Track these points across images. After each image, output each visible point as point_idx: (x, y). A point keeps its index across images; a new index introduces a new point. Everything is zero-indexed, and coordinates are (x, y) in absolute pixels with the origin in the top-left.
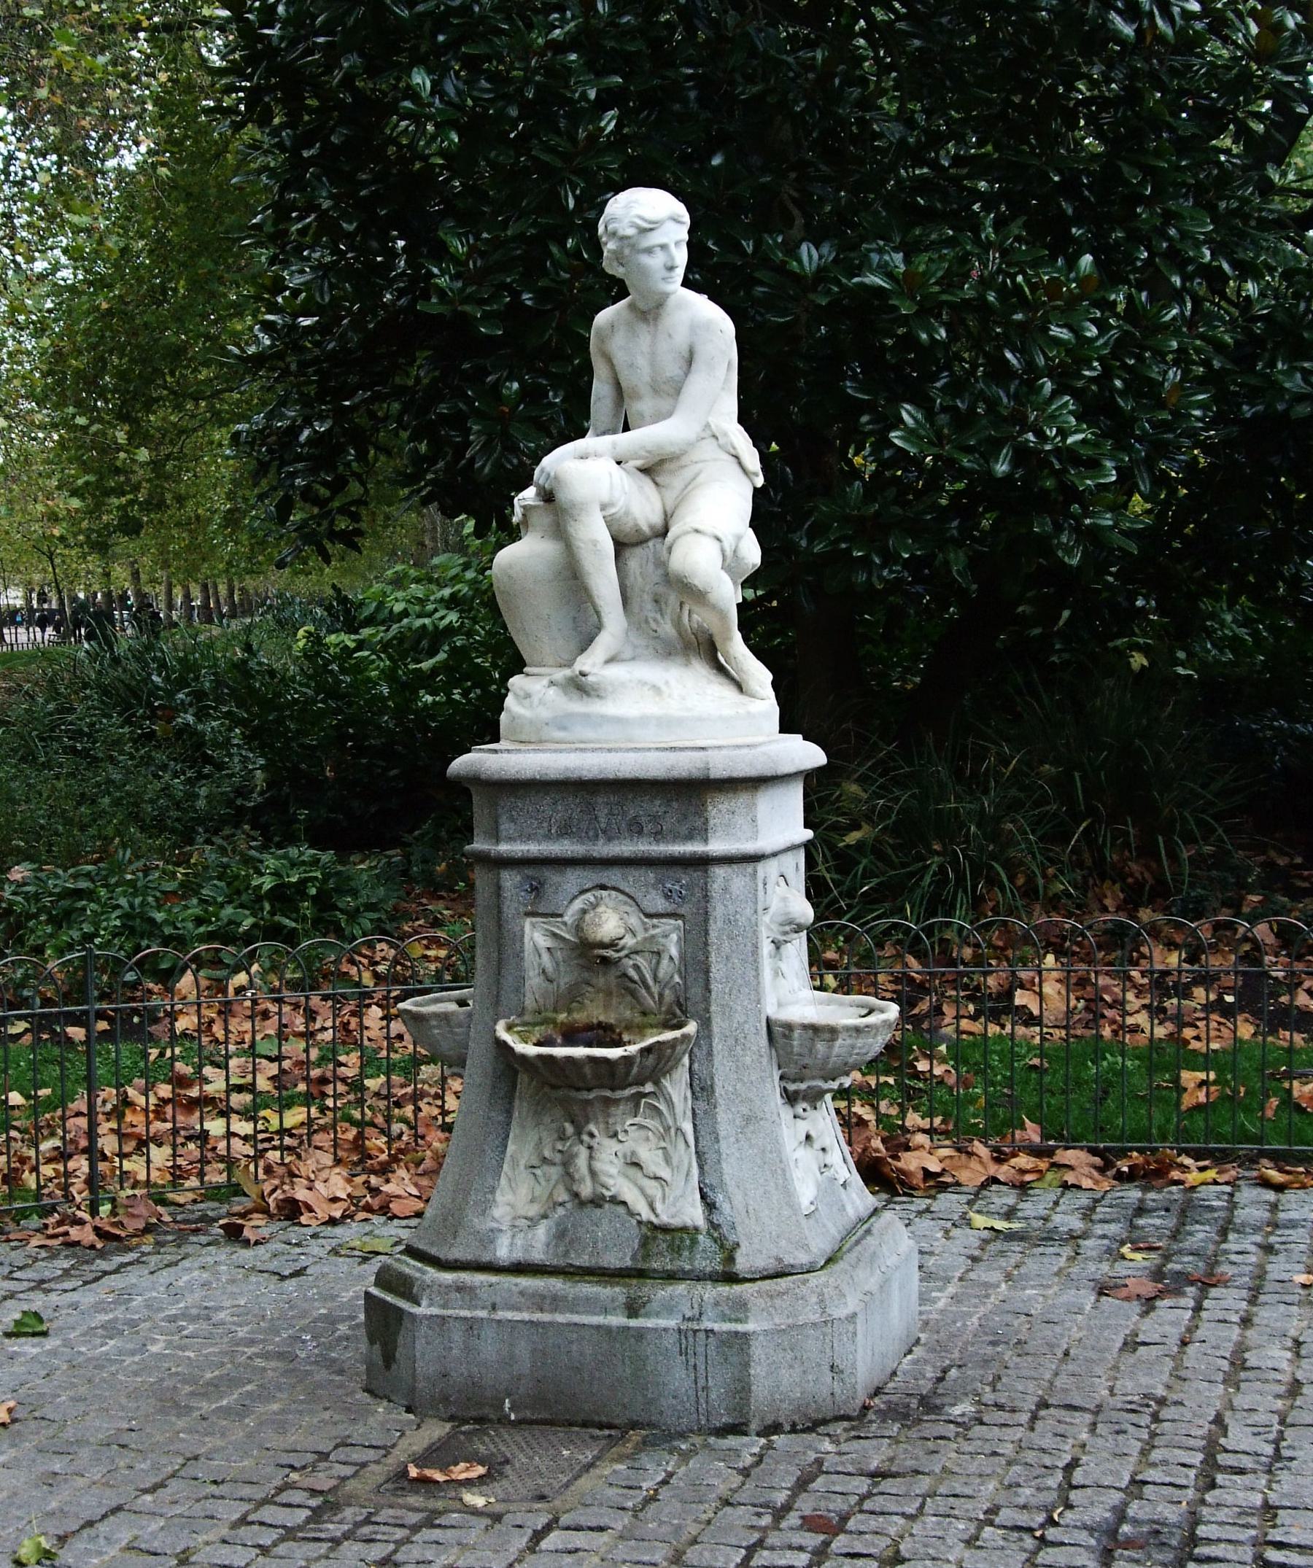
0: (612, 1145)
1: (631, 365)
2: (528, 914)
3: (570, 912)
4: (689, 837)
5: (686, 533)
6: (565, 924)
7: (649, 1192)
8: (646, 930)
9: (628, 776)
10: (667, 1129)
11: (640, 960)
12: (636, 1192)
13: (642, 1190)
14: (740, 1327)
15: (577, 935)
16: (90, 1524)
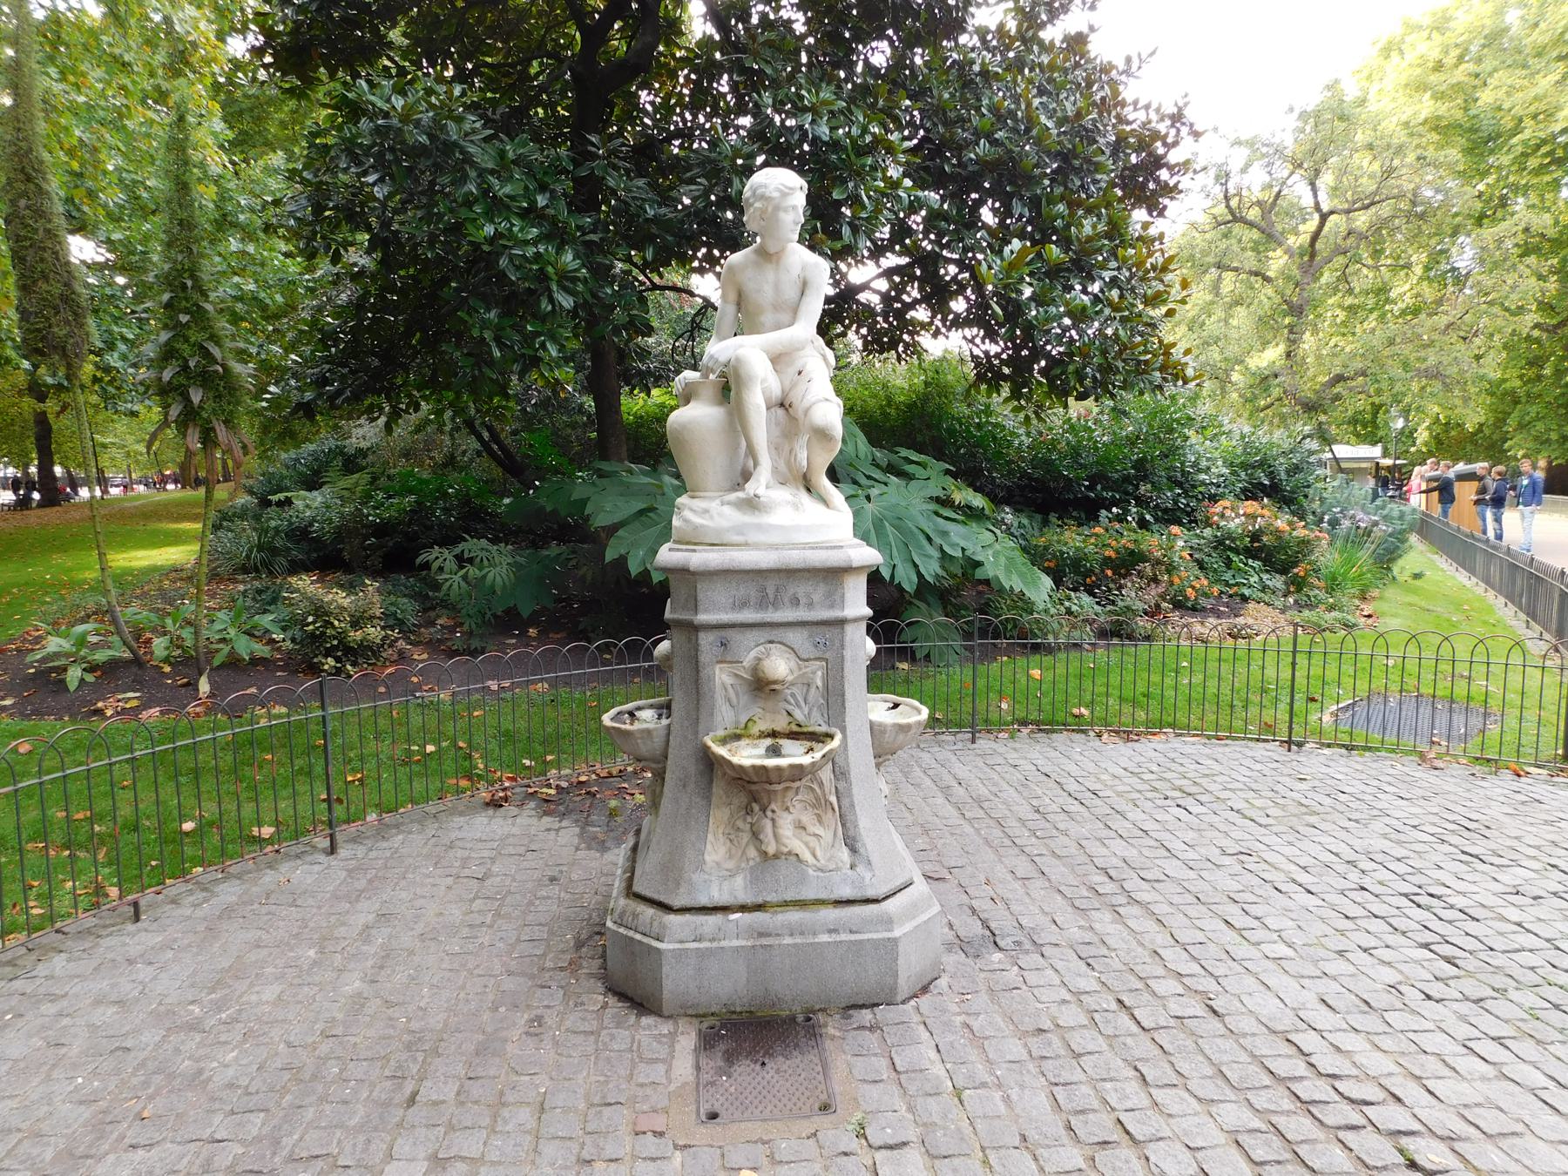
0: (785, 814)
4: (832, 606)
9: (836, 564)
11: (795, 690)
13: (806, 844)
14: (889, 935)
16: (1279, 1162)
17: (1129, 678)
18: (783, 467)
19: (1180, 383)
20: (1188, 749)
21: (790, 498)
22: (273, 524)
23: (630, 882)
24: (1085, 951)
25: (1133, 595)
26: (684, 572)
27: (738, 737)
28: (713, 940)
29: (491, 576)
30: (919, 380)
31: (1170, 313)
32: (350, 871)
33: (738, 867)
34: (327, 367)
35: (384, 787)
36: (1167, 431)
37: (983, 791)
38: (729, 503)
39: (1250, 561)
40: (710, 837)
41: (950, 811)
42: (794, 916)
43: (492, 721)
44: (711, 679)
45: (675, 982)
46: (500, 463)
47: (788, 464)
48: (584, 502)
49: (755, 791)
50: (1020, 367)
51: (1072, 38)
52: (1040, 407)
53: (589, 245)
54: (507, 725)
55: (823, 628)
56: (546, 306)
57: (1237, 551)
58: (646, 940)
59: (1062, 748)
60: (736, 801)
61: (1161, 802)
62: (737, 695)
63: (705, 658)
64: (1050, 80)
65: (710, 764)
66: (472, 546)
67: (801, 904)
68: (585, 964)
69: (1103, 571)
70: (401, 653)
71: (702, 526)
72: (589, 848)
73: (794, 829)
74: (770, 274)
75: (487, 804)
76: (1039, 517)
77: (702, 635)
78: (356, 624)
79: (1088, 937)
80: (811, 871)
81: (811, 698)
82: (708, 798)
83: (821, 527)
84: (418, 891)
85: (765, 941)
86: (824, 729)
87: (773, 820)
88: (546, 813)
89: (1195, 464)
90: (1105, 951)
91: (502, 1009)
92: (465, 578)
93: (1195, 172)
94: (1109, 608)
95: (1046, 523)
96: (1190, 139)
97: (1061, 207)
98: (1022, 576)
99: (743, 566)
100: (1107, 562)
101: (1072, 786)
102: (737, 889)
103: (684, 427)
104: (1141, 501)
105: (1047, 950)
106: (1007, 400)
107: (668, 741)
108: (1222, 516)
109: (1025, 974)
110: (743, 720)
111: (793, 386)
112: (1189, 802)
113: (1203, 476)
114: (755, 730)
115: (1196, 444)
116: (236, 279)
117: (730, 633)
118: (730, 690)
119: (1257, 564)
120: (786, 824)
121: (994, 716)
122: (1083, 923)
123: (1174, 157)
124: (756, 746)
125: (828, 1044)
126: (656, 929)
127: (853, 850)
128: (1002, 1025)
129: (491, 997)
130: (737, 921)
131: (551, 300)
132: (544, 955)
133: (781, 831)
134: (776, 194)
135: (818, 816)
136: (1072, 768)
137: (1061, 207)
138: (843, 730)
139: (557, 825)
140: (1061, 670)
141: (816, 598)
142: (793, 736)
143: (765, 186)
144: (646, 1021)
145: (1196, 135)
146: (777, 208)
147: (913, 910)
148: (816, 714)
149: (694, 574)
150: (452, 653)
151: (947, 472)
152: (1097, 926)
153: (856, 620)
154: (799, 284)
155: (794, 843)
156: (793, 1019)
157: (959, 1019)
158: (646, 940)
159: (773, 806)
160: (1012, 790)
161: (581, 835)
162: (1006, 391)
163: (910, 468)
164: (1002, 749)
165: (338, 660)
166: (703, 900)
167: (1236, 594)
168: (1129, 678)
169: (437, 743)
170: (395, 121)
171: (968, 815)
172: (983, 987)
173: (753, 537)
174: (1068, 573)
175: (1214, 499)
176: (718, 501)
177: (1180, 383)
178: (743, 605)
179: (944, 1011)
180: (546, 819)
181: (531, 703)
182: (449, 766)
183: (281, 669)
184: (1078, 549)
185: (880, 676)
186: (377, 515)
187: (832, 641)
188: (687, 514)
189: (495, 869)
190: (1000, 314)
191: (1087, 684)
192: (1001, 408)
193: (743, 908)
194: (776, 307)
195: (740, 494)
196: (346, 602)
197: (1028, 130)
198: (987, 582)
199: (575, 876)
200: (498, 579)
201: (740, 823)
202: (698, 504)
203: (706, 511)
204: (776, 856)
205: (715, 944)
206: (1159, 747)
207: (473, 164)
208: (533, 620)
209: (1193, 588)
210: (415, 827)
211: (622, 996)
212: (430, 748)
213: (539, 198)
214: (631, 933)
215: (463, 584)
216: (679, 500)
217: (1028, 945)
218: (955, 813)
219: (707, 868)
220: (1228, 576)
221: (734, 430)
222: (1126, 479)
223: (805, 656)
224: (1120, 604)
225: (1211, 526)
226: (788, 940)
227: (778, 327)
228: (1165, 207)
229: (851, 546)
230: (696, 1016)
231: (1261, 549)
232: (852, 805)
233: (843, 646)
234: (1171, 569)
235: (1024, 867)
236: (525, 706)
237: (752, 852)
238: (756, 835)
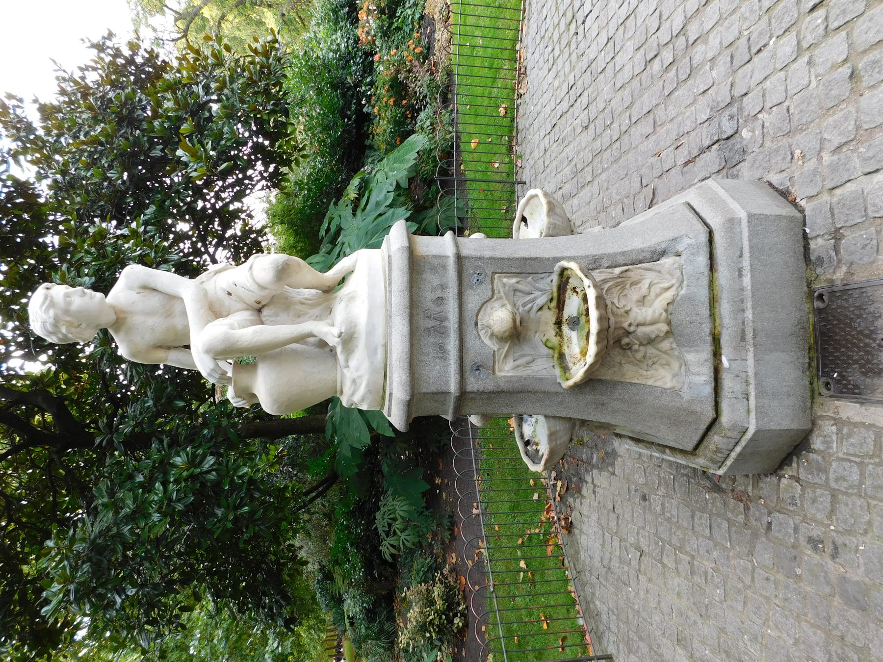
0: (632, 314)
1: (153, 330)
2: (494, 373)
3: (492, 346)
4: (444, 267)
5: (252, 275)
6: (499, 349)
7: (658, 291)
8: (501, 298)
9: (406, 262)
10: (617, 285)
11: (519, 303)
12: (660, 299)
13: (658, 296)
15: (506, 342)
17: (477, 81)
18: (316, 311)
19: (277, 45)
20: (533, 29)
21: (343, 304)
22: (363, 630)
23: (683, 452)
24: (742, 55)
25: (420, 84)
26: (409, 405)
27: (562, 356)
28: (747, 383)
29: (402, 513)
30: (278, 228)
31: (228, 49)
32: (630, 651)
33: (678, 358)
34: (261, 610)
35: (553, 603)
36: (314, 70)
37: (567, 171)
38: (347, 361)
39: (397, 15)
40: (650, 382)
41: (586, 193)
42: (725, 308)
43: (502, 519)
44: (509, 379)
45: (785, 419)
46: (331, 485)
47: (313, 306)
48: (352, 448)
49: (616, 341)
50: (268, 157)
51: (42, 115)
52: (295, 148)
53: (170, 446)
54: (506, 507)
55: (464, 275)
56: (213, 476)
57: (391, 24)
58: (743, 443)
59: (531, 120)
60: (618, 359)
61: (580, 37)
62: (523, 356)
63: (490, 386)
64: (69, 129)
65: (590, 381)
66: (380, 522)
67: (713, 301)
68: (741, 488)
69: (403, 106)
70: (451, 571)
71: (367, 386)
72: (613, 465)
73: (648, 303)
74: (137, 320)
75: (570, 532)
76: (367, 152)
77: (469, 388)
78: (431, 603)
79: (725, 58)
80: (683, 292)
81: (527, 289)
82: (615, 384)
83: (371, 275)
84: (653, 605)
85: (749, 335)
86: (555, 277)
87: (638, 325)
88: (579, 491)
89: (335, 52)
90: (743, 41)
91: (799, 571)
92: (402, 531)
93: (138, 38)
94: (428, 99)
95: (371, 147)
96: (114, 40)
97: (156, 123)
98: (406, 153)
100: (397, 104)
101: (565, 105)
102: (698, 361)
103: (275, 401)
104: (358, 84)
105: (737, 92)
106: (291, 169)
107: (560, 418)
108: (368, 33)
109: (768, 105)
110: (545, 351)
111: (241, 300)
112: (580, 17)
113: (342, 46)
114: (555, 340)
115: (323, 51)
116: (215, 641)
117: (468, 363)
118: (518, 363)
119: (399, 11)
120: (641, 314)
121: (505, 168)
122: (707, 68)
123: (127, 52)
124: (569, 340)
125: (860, 277)
126: (735, 434)
127: (663, 253)
128: (840, 114)
129: (781, 577)
130: (729, 360)
131: (208, 472)
132: (729, 520)
133: (649, 318)
134: (52, 312)
135: (632, 284)
136: (548, 110)
137: (156, 123)
138: (557, 260)
139: (590, 485)
140: (471, 129)
141: (436, 281)
142: (561, 305)
143: (44, 323)
144: (817, 443)
145: (110, 36)
146: (67, 312)
147: (714, 201)
148: (541, 285)
149: (412, 395)
150: (453, 537)
151: (336, 204)
152: (710, 55)
153: (457, 245)
154: (147, 292)
155: (655, 308)
156: (819, 312)
157: (827, 158)
158: (743, 443)
159: (625, 325)
160: (567, 150)
161: (600, 469)
162: (284, 169)
163: (333, 228)
164: (531, 162)
165: (455, 615)
166: (708, 390)
167: (419, 23)
168: (477, 81)
169: (518, 560)
170: (72, 587)
171: (589, 179)
172: (785, 141)
173: (379, 339)
174: (403, 131)
175: (357, 40)
176: (345, 371)
177: (277, 45)
178: (442, 349)
179: (815, 172)
180: (584, 491)
181: (490, 489)
182: (536, 552)
183: (460, 651)
184: (389, 122)
185: (502, 224)
186: (360, 569)
187: (476, 268)
188: (356, 398)
189: (632, 540)
190: (228, 165)
191: (481, 110)
192: (298, 173)
193: (717, 354)
194: (169, 314)
195: (339, 350)
196: (417, 609)
197: (101, 144)
198: (411, 180)
199: (642, 481)
200: (404, 508)
201: (639, 356)
202: (347, 389)
203: (354, 381)
204: (669, 323)
205: (752, 381)
206: (531, 51)
207: (109, 529)
208: (430, 480)
209: (414, 49)
210: (588, 589)
211: (785, 461)
212: (522, 564)
213: (138, 480)
214: (734, 455)
215: (407, 533)
216: (344, 404)
217: (734, 110)
218: (587, 189)
219: (678, 386)
220: (407, 29)
221: (280, 353)
222: (344, 95)
223: (490, 293)
224: (425, 92)
225: (374, 41)
226: (749, 314)
227: (184, 314)
228: (164, 61)
229: (389, 249)
230: (813, 398)
231: (390, 8)
232: (623, 253)
233: (481, 258)
234: (402, 61)
235: (645, 127)
236: (492, 494)
237: (666, 345)
238: (651, 341)
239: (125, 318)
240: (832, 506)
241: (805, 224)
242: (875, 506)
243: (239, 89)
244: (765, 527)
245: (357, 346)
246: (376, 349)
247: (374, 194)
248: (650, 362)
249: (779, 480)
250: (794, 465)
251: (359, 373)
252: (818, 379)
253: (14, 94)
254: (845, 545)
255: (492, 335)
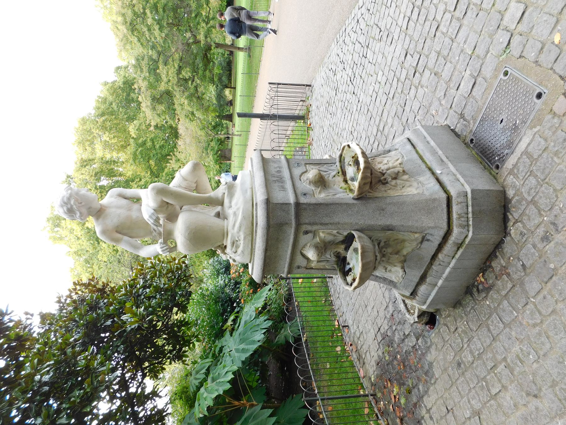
38: (230, 202)
55: (290, 164)
58: (470, 203)
71: (243, 213)
85: (445, 159)
99: (263, 179)
114: (346, 186)
134: (69, 192)
142: (344, 173)
143: (63, 197)
154: (120, 198)
158: (470, 203)
166: (438, 186)
173: (248, 185)
211: (505, 220)
214: (470, 215)
219: (421, 192)
239: (105, 210)
240: (537, 209)
241: (450, 127)
242: (549, 180)
243: (156, 342)
244: (522, 270)
245: (236, 191)
246: (246, 190)
247: (243, 318)
248: (401, 187)
249: (510, 235)
250: (510, 217)
251: (238, 206)
252: (492, 169)
253: (29, 312)
254: (556, 216)
255: (310, 182)
